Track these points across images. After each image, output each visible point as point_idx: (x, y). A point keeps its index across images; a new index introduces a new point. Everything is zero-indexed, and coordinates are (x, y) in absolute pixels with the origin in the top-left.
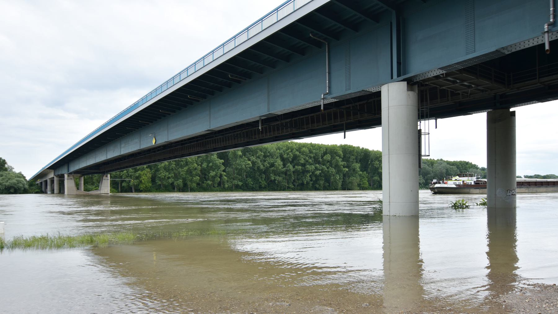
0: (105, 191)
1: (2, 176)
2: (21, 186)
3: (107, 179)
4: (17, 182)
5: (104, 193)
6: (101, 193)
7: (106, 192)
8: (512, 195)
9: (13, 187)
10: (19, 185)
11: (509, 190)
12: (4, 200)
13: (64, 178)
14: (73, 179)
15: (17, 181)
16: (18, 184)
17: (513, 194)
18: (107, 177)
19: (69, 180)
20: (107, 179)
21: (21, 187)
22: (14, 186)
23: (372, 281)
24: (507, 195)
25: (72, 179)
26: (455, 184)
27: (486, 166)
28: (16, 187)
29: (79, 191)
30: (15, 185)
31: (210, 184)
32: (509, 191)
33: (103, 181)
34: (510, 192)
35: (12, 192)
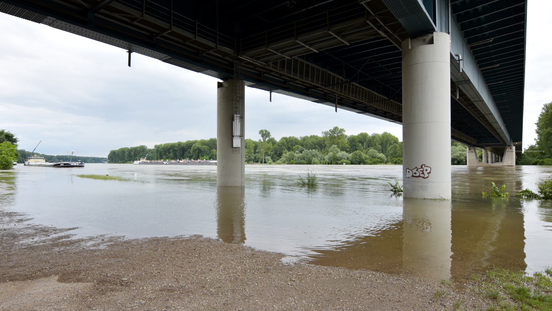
0: (508, 164)
1: (1, 146)
2: (463, 158)
3: (512, 151)
4: (459, 155)
5: (507, 165)
6: (504, 165)
7: (510, 165)
8: (413, 176)
9: (457, 159)
10: (461, 157)
11: (408, 169)
12: (338, 169)
13: (516, 152)
14: (474, 152)
15: (460, 154)
16: (460, 156)
17: (415, 175)
18: (511, 149)
19: (470, 153)
20: (511, 151)
21: (463, 159)
22: (457, 158)
23: (393, 221)
24: (406, 176)
25: (473, 152)
26: (141, 154)
27: (245, 86)
28: (458, 159)
29: (480, 163)
30: (458, 157)
31: (352, 155)
32: (408, 170)
33: (507, 153)
34: (409, 172)
35: (456, 163)
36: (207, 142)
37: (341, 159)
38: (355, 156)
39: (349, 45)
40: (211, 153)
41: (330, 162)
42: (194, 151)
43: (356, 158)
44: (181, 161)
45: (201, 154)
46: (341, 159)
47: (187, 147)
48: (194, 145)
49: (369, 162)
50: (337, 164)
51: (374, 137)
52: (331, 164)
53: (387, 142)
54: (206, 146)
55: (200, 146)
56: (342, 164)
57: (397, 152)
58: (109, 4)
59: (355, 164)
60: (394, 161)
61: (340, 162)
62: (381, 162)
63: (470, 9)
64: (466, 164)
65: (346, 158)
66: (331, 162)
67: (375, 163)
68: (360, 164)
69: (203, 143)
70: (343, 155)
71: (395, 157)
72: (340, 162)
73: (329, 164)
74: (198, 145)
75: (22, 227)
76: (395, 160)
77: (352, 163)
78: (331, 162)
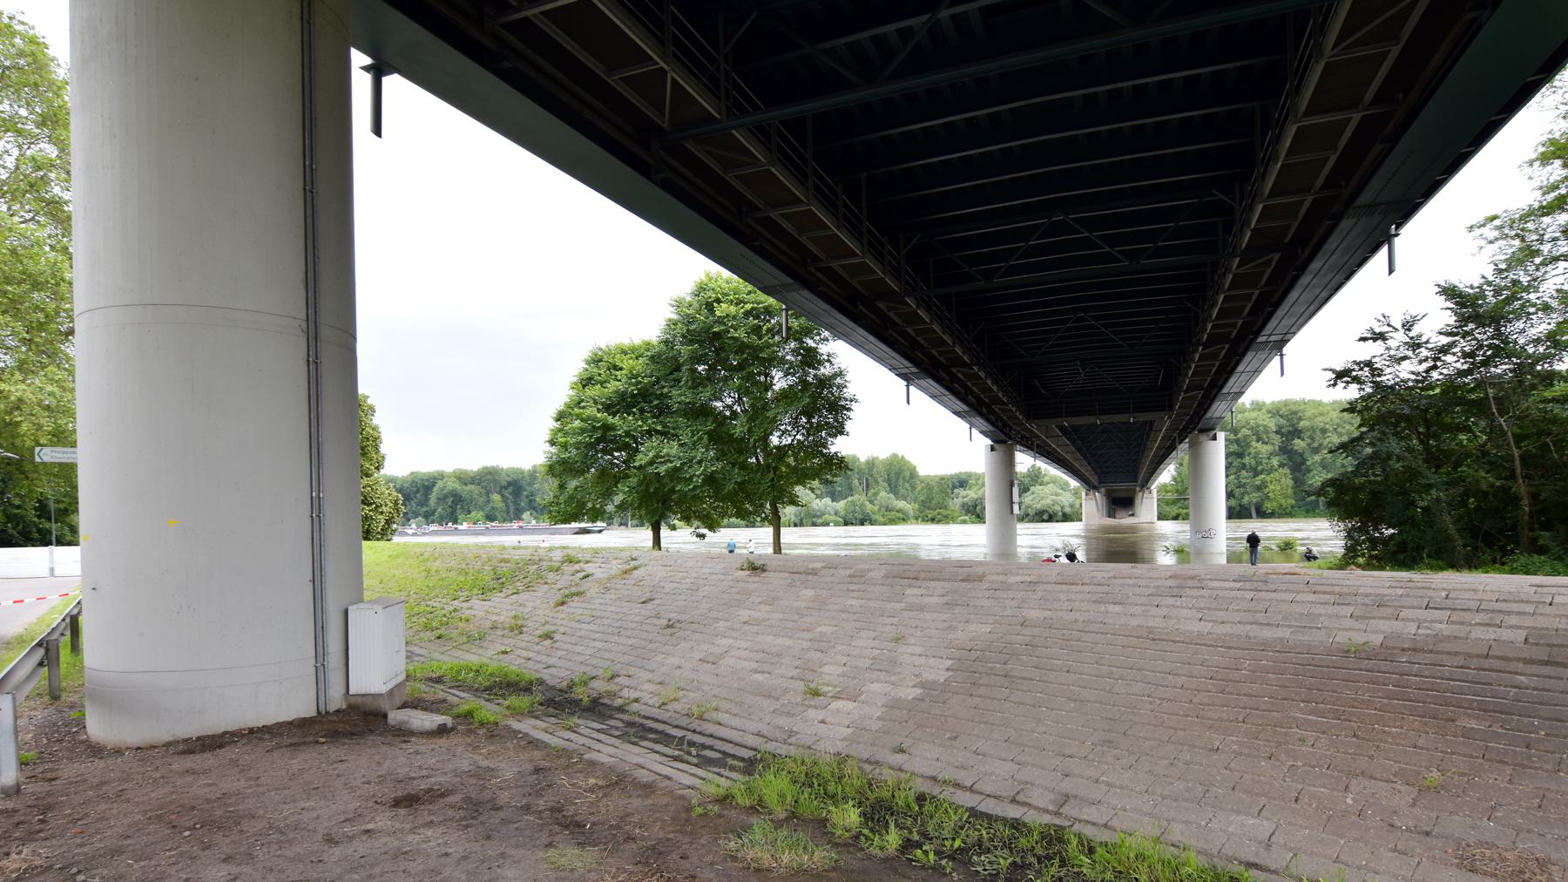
36: (472, 475)
37: (823, 514)
38: (852, 508)
39: (734, 132)
40: (491, 505)
41: (798, 522)
42: (442, 499)
43: (853, 512)
44: (460, 527)
45: (462, 508)
46: (823, 514)
47: (414, 489)
48: (440, 484)
49: (881, 519)
50: (814, 524)
51: (871, 464)
52: (802, 525)
53: (898, 474)
54: (473, 486)
55: (458, 486)
56: (826, 524)
57: (933, 498)
58: (734, 132)
59: (852, 524)
60: (930, 516)
61: (820, 521)
62: (903, 518)
63: (1290, 146)
64: (1081, 520)
65: (833, 513)
66: (801, 520)
67: (892, 522)
68: (863, 524)
69: (463, 478)
70: (826, 506)
71: (929, 508)
72: (820, 521)
73: (795, 525)
74: (453, 485)
75: (1070, 617)
76: (931, 514)
77: (846, 524)
78: (801, 520)
